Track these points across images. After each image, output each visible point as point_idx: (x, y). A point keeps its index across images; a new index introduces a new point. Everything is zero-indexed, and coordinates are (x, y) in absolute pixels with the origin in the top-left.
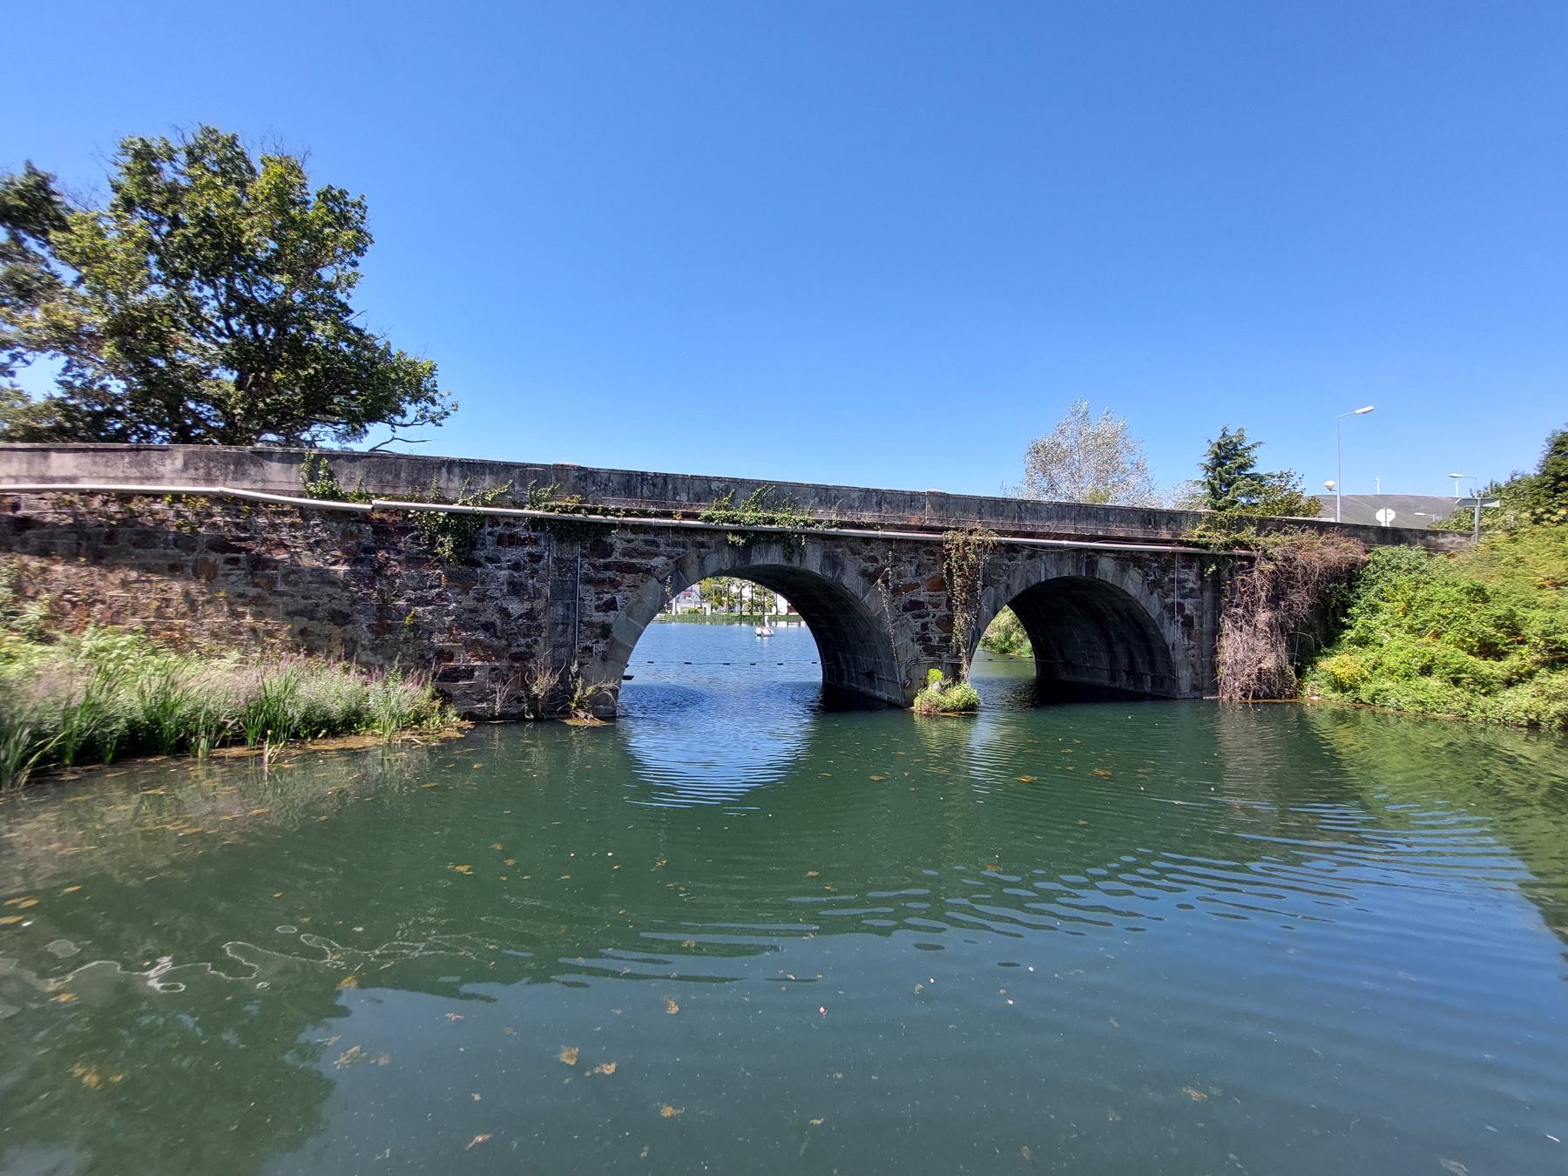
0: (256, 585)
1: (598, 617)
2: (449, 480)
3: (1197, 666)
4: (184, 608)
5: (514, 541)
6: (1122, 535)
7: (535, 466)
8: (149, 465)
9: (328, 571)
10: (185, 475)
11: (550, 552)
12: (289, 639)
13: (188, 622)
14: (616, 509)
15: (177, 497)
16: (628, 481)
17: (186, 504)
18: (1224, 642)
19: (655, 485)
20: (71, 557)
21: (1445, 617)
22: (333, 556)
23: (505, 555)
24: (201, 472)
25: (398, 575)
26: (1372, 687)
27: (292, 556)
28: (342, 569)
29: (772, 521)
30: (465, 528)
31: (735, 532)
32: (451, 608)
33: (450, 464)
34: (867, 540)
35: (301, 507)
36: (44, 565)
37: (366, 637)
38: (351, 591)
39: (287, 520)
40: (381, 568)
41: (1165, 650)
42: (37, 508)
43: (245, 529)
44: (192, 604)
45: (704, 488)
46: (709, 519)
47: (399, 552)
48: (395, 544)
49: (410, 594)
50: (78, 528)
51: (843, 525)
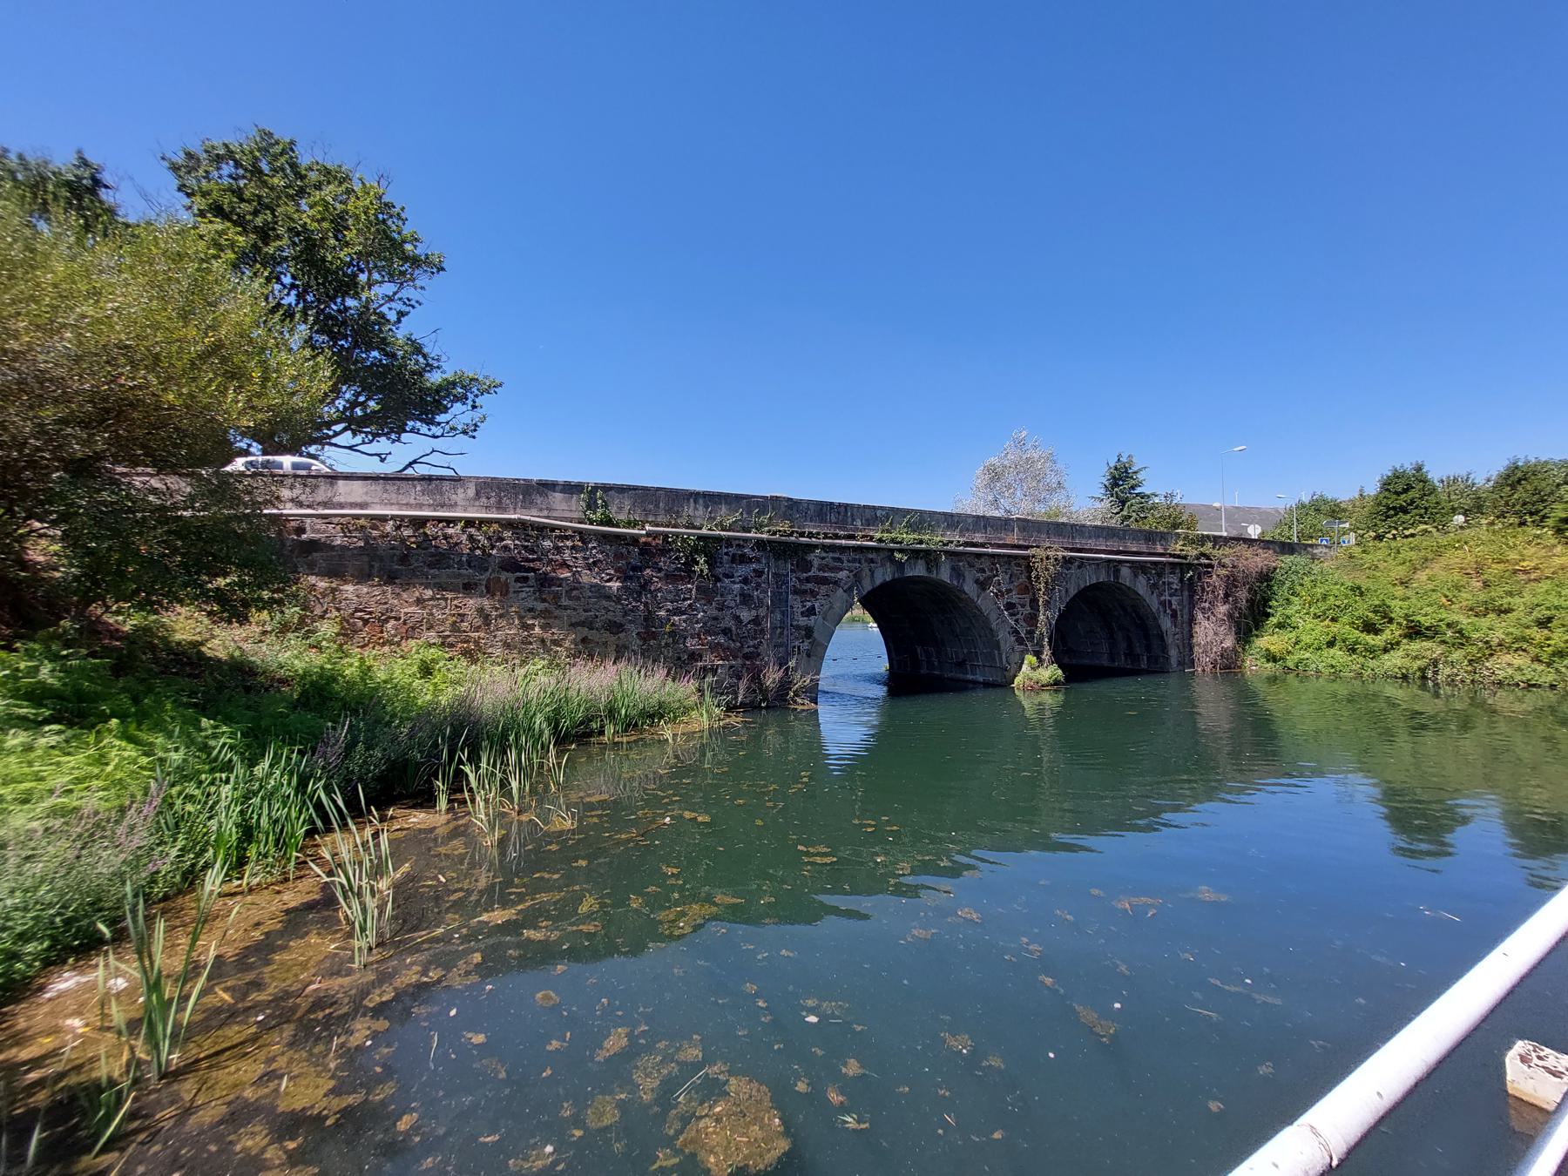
0: (544, 601)
1: (803, 621)
2: (696, 509)
3: (1181, 647)
4: (478, 622)
5: (743, 559)
6: (1135, 549)
7: (758, 497)
8: (441, 494)
9: (604, 587)
10: (477, 503)
11: (770, 568)
12: (572, 646)
13: (482, 635)
14: (815, 532)
15: (469, 523)
16: (821, 509)
17: (479, 529)
18: (1197, 629)
19: (839, 513)
20: (363, 577)
21: (1338, 607)
22: (607, 574)
23: (737, 571)
24: (492, 500)
25: (659, 590)
26: (1296, 657)
27: (574, 574)
28: (615, 585)
29: (921, 542)
30: (709, 546)
31: (901, 551)
32: (699, 616)
33: (695, 496)
34: (979, 556)
35: (580, 532)
36: (334, 585)
37: (636, 643)
38: (622, 604)
39: (569, 543)
40: (646, 584)
41: (1161, 637)
42: (324, 532)
43: (533, 552)
44: (486, 619)
45: (873, 515)
46: (880, 540)
47: (660, 570)
48: (656, 563)
49: (669, 606)
50: (370, 550)
51: (967, 544)
